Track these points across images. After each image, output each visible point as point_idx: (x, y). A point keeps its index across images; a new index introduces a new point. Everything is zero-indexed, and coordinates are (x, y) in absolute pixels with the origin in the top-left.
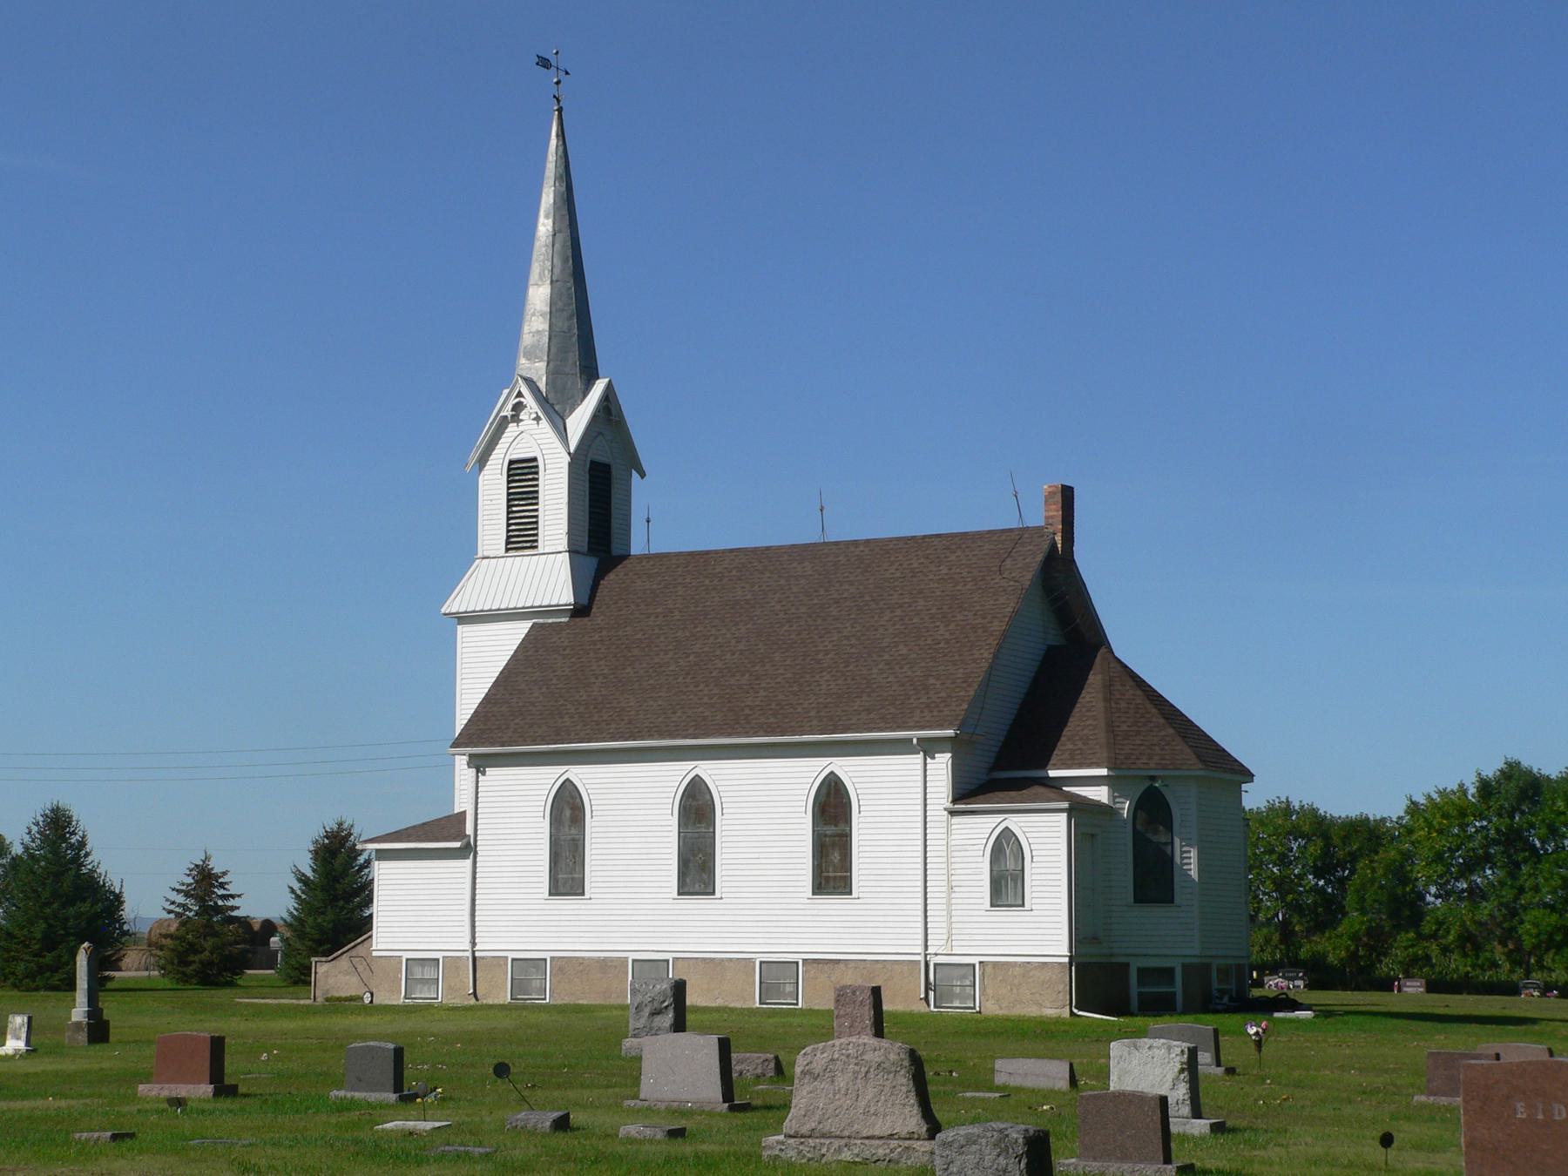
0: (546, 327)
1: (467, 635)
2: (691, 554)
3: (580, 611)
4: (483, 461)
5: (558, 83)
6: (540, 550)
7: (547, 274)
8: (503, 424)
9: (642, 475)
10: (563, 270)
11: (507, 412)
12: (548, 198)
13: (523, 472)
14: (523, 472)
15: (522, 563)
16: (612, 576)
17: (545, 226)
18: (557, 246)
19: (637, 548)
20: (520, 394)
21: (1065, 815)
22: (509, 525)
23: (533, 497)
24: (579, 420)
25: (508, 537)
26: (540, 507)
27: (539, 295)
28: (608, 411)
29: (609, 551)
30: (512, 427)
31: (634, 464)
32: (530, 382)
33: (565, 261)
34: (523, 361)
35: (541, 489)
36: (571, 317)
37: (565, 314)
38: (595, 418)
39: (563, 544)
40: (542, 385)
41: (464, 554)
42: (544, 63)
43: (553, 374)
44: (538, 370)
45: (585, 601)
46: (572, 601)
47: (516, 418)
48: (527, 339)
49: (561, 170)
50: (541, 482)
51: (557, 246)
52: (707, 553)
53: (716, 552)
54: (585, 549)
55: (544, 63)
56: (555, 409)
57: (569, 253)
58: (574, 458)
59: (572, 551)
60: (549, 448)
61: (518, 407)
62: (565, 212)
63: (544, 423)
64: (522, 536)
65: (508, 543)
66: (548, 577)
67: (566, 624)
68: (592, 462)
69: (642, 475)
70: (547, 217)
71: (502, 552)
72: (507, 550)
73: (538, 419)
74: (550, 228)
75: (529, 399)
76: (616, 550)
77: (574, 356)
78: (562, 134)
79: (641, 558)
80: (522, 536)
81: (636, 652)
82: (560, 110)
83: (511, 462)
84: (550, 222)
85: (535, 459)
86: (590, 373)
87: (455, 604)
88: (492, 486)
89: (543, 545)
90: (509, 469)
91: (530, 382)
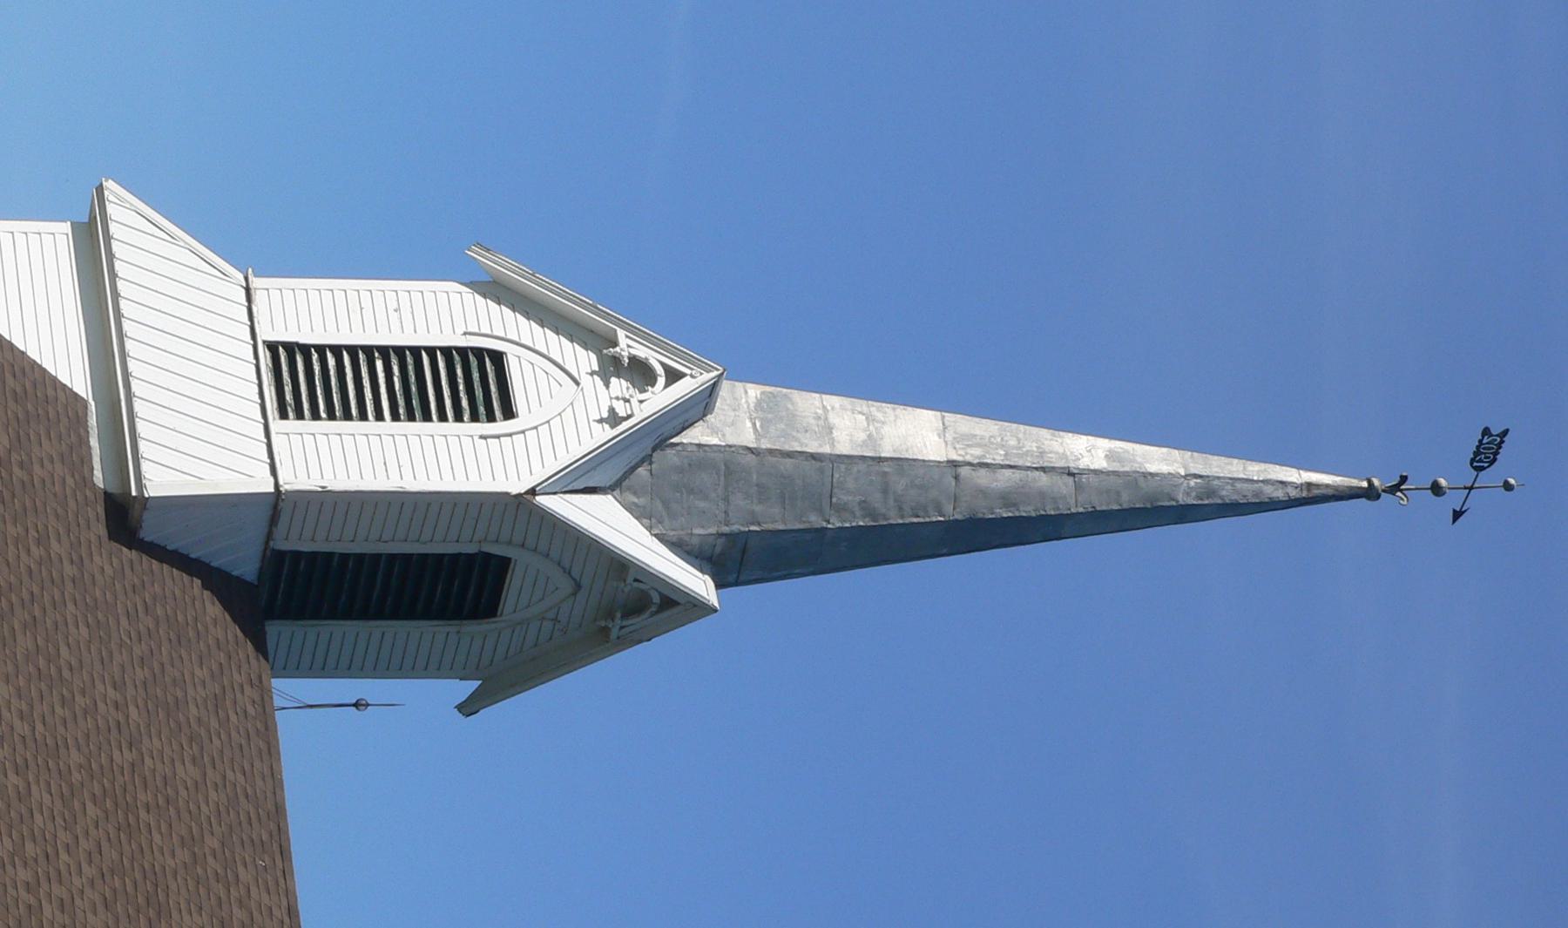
0: (844, 448)
1: (48, 246)
2: (279, 811)
3: (124, 515)
4: (496, 290)
5: (1436, 489)
6: (276, 425)
7: (974, 454)
8: (598, 341)
9: (468, 708)
10: (983, 492)
11: (628, 346)
12: (1159, 461)
13: (472, 385)
14: (472, 385)
15: (241, 383)
16: (214, 608)
17: (1090, 452)
18: (1043, 480)
19: (285, 689)
20: (673, 376)
21: (271, 489)
22: (337, 350)
23: (414, 406)
24: (608, 521)
25: (305, 349)
26: (388, 425)
27: (919, 434)
28: (638, 606)
29: (272, 613)
30: (584, 360)
31: (496, 683)
32: (703, 404)
33: (1006, 498)
34: (754, 391)
35: (435, 426)
36: (870, 512)
37: (876, 499)
38: (620, 566)
39: (295, 478)
40: (697, 435)
41: (257, 242)
42: (1487, 452)
43: (727, 465)
44: (738, 420)
45: (148, 533)
46: (152, 491)
47: (611, 367)
48: (808, 404)
49: (1228, 495)
50: (451, 427)
51: (1043, 480)
52: (285, 853)
53: (287, 873)
54: (281, 544)
55: (1487, 452)
56: (636, 462)
57: (1027, 510)
58: (520, 509)
59: (277, 503)
60: (551, 431)
61: (640, 374)
62: (1126, 501)
63: (605, 434)
64: (309, 380)
65: (290, 348)
66: (204, 439)
67: (87, 481)
68: (504, 564)
69: (468, 708)
70: (1110, 456)
71: (266, 333)
72: (272, 347)
73: (613, 419)
74: (1086, 462)
75: (660, 398)
76: (277, 631)
77: (776, 519)
78: (1313, 497)
79: (265, 694)
80: (309, 380)
81: (24, 642)
82: (1371, 493)
83: (498, 358)
84: (1100, 463)
85: (509, 413)
86: (732, 561)
87: (128, 218)
88: (433, 313)
89: (293, 435)
90: (479, 352)
91: (703, 404)
